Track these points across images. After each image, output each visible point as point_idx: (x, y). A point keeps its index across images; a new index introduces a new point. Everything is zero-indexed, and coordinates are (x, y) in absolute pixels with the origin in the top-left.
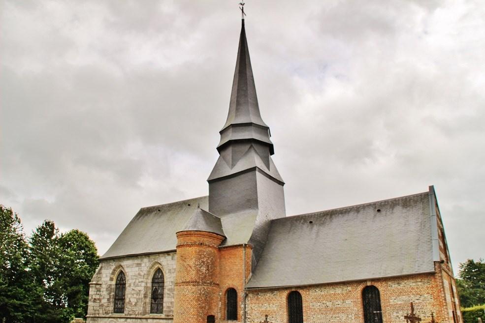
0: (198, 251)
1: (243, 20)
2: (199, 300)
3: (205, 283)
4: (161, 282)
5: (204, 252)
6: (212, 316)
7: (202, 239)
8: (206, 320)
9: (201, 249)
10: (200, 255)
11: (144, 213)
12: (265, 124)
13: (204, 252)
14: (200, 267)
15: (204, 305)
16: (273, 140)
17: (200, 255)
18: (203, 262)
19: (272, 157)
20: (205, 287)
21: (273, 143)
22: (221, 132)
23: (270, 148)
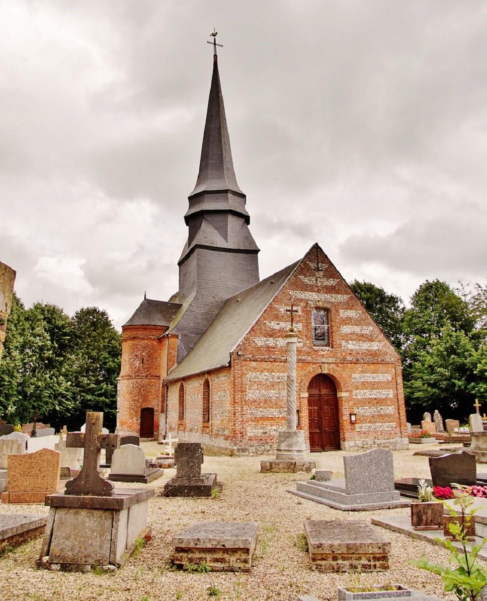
0: (131, 345)
1: (215, 56)
2: (131, 393)
3: (138, 376)
4: (472, 470)
5: (138, 345)
6: (148, 409)
7: (134, 333)
8: (140, 413)
9: (135, 342)
10: (134, 349)
11: (180, 264)
12: (240, 190)
13: (138, 345)
14: (133, 361)
15: (136, 398)
16: (250, 209)
17: (134, 349)
18: (136, 355)
19: (249, 226)
20: (139, 381)
21: (250, 215)
22: (191, 199)
23: (247, 219)
